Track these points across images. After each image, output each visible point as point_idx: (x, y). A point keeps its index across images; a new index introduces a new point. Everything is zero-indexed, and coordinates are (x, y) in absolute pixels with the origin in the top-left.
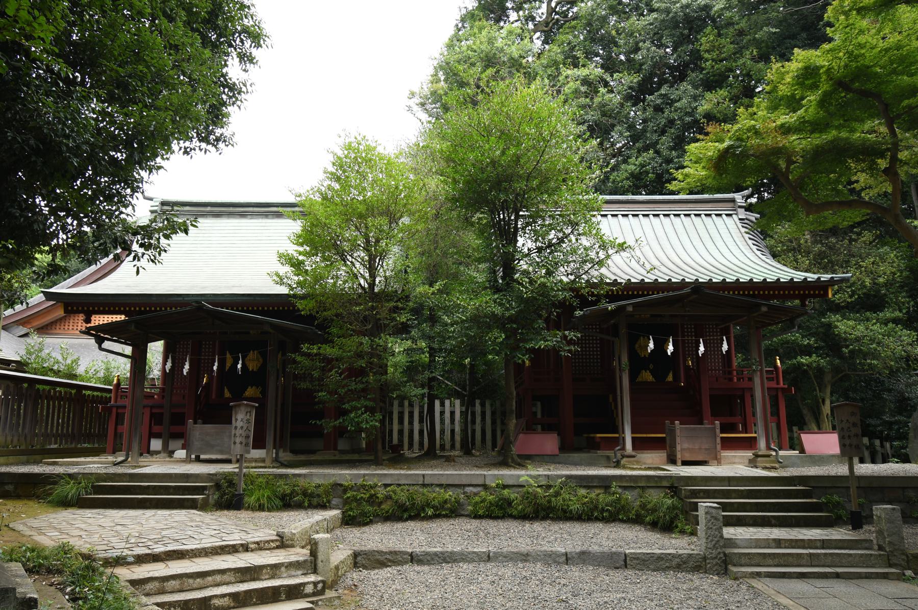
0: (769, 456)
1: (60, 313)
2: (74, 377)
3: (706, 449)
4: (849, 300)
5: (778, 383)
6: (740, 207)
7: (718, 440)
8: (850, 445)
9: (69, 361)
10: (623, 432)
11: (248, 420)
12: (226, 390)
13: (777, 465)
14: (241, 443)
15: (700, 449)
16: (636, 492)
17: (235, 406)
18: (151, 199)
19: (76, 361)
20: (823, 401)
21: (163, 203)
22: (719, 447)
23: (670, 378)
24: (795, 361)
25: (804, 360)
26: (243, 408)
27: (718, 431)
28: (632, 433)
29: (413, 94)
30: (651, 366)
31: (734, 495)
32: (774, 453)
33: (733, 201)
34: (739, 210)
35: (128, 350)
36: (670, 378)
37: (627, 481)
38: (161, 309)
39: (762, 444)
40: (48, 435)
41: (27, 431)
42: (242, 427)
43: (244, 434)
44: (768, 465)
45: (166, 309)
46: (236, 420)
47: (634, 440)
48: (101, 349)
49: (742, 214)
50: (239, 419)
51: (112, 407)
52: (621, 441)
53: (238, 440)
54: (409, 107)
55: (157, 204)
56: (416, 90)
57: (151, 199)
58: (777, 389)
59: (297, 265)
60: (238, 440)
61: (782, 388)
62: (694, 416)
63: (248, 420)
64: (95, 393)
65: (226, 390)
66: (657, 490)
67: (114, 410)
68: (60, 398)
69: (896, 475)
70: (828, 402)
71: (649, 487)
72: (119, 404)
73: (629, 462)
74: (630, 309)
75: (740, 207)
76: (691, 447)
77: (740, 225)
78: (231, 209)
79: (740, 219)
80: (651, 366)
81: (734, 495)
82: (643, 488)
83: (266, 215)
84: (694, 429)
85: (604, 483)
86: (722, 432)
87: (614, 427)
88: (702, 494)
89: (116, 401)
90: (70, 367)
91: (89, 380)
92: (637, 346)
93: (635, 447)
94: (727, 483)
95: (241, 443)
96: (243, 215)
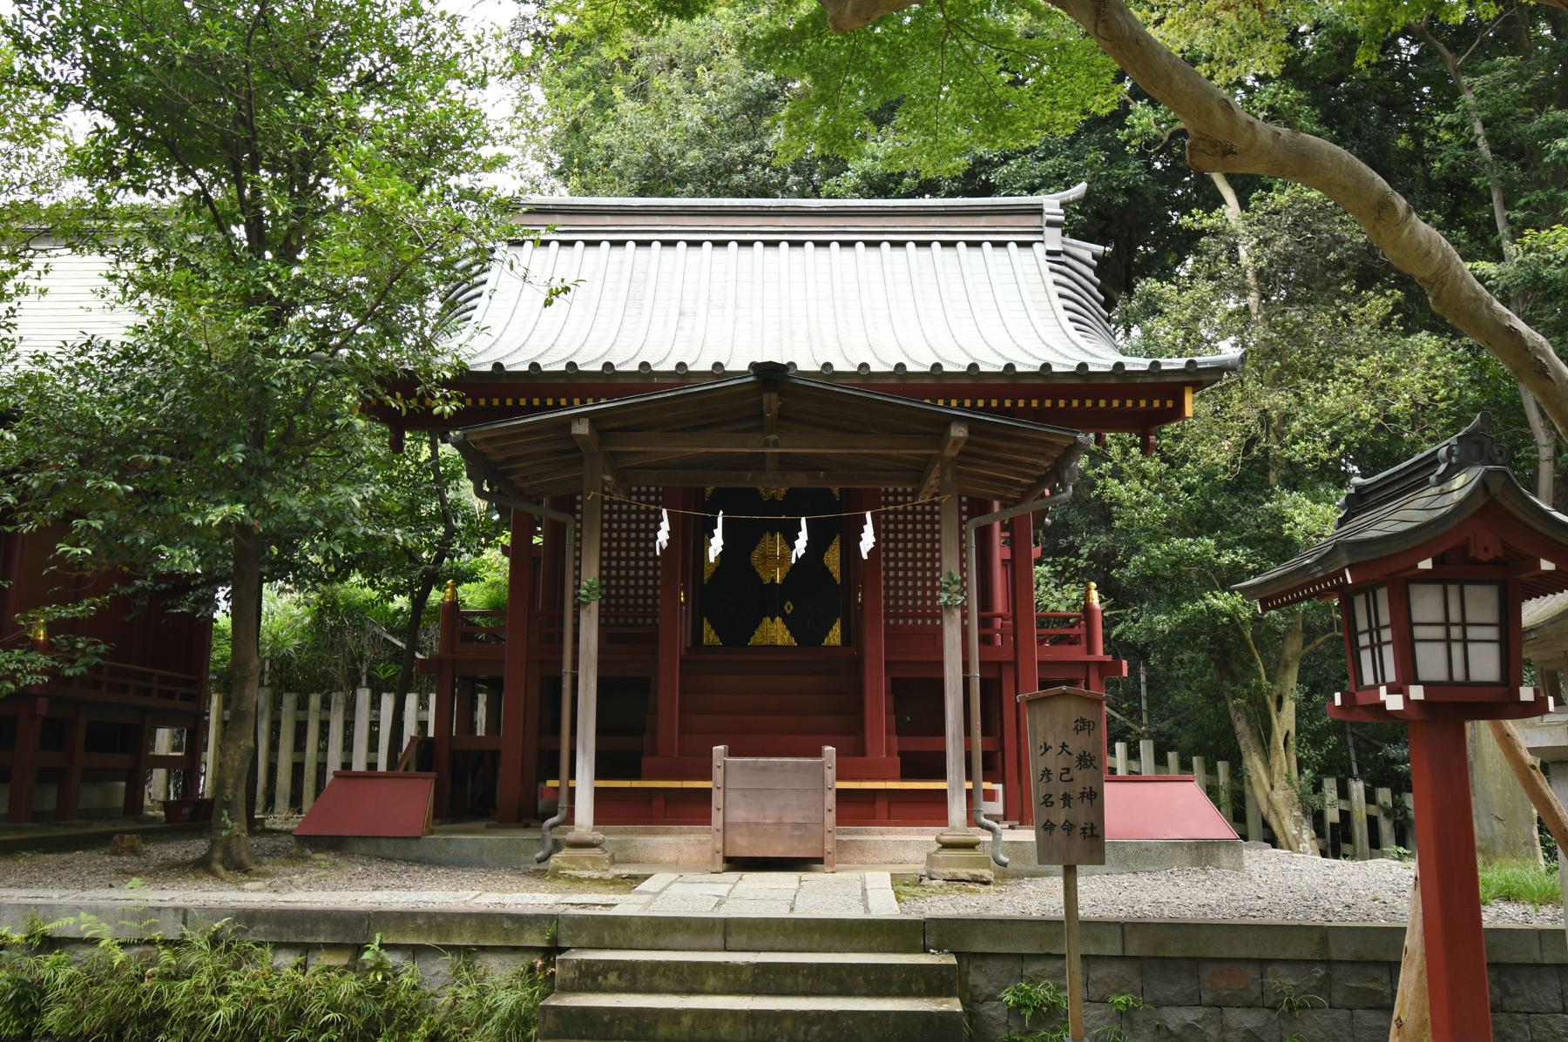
0: (971, 846)
3: (797, 826)
4: (1325, 456)
5: (1090, 649)
6: (1051, 224)
7: (831, 799)
8: (1069, 827)
10: (572, 776)
13: (987, 874)
15: (780, 824)
16: (442, 967)
20: (1280, 702)
22: (830, 818)
23: (834, 637)
24: (1201, 605)
25: (1221, 601)
27: (830, 774)
28: (598, 776)
30: (789, 607)
31: (711, 982)
32: (987, 837)
33: (1038, 211)
34: (1047, 230)
36: (834, 637)
37: (418, 930)
39: (957, 809)
44: (963, 873)
47: (600, 795)
49: (1054, 239)
52: (563, 803)
58: (1087, 664)
61: (1100, 664)
62: (770, 732)
66: (508, 959)
69: (1212, 917)
70: (1289, 707)
71: (483, 949)
73: (572, 860)
74: (581, 429)
75: (1051, 224)
76: (753, 818)
77: (1045, 266)
79: (1049, 253)
80: (789, 607)
81: (711, 982)
82: (465, 951)
84: (765, 768)
85: (348, 933)
86: (839, 778)
87: (550, 761)
88: (613, 978)
92: (755, 556)
93: (600, 818)
94: (718, 940)
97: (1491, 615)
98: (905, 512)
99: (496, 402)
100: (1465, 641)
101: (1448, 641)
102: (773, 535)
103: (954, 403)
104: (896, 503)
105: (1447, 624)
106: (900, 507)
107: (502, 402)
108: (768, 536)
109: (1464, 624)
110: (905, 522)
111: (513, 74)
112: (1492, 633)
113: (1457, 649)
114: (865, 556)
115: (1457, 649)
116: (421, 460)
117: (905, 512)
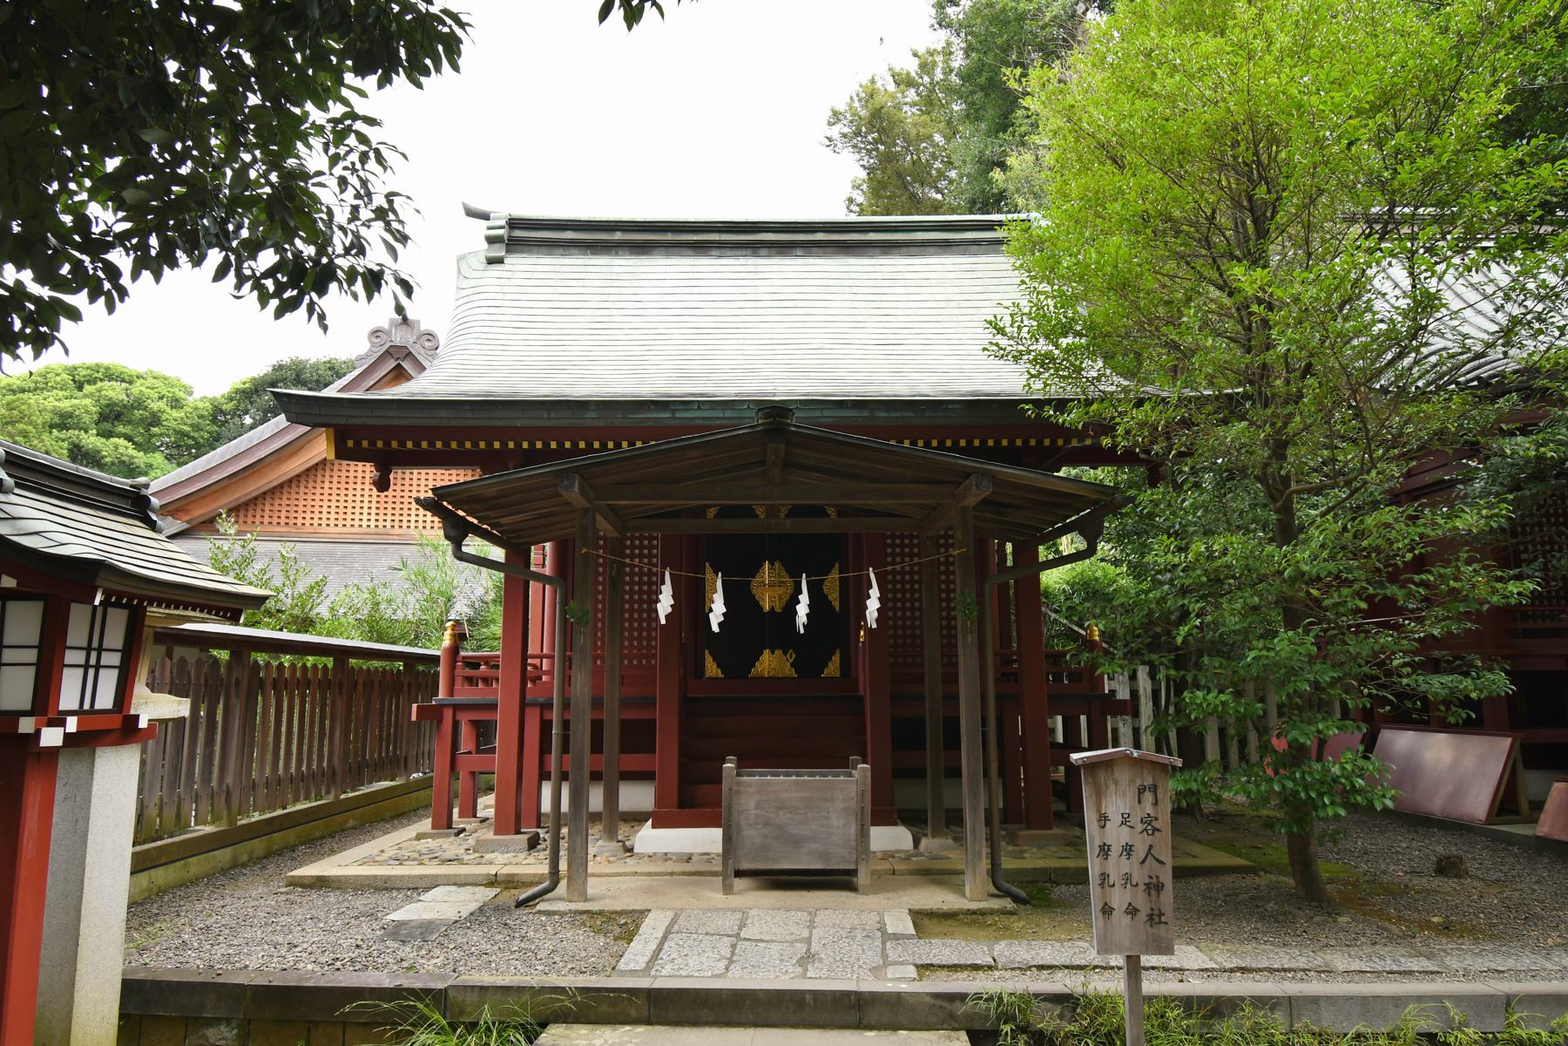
1: (321, 448)
2: (306, 624)
9: (301, 588)
11: (1148, 820)
12: (709, 660)
14: (1132, 911)
17: (1092, 766)
18: (485, 216)
19: (319, 587)
21: (514, 223)
26: (1123, 775)
29: (836, 116)
35: (497, 553)
38: (604, 446)
40: (279, 782)
41: (230, 780)
42: (1128, 850)
43: (1139, 876)
45: (618, 445)
46: (1103, 819)
48: (460, 556)
50: (1115, 818)
51: (441, 707)
53: (1119, 898)
54: (830, 139)
55: (503, 223)
56: (842, 107)
57: (485, 216)
59: (1123, 287)
60: (1119, 898)
63: (1148, 820)
64: (376, 664)
65: (709, 660)
67: (448, 714)
68: (304, 681)
72: (459, 698)
78: (669, 237)
83: (754, 248)
89: (451, 693)
90: (304, 600)
91: (306, 624)
95: (1132, 911)
96: (701, 248)
97: (33, 637)
98: (903, 572)
99: (539, 445)
100: (98, 667)
101: (86, 667)
102: (772, 608)
103: (921, 443)
104: (894, 563)
105: (89, 649)
106: (898, 567)
107: (546, 445)
108: (778, 610)
109: (100, 650)
110: (903, 582)
111: (949, 26)
112: (31, 656)
113: (91, 672)
114: (715, 629)
115: (91, 672)
116: (599, 518)
117: (903, 572)
